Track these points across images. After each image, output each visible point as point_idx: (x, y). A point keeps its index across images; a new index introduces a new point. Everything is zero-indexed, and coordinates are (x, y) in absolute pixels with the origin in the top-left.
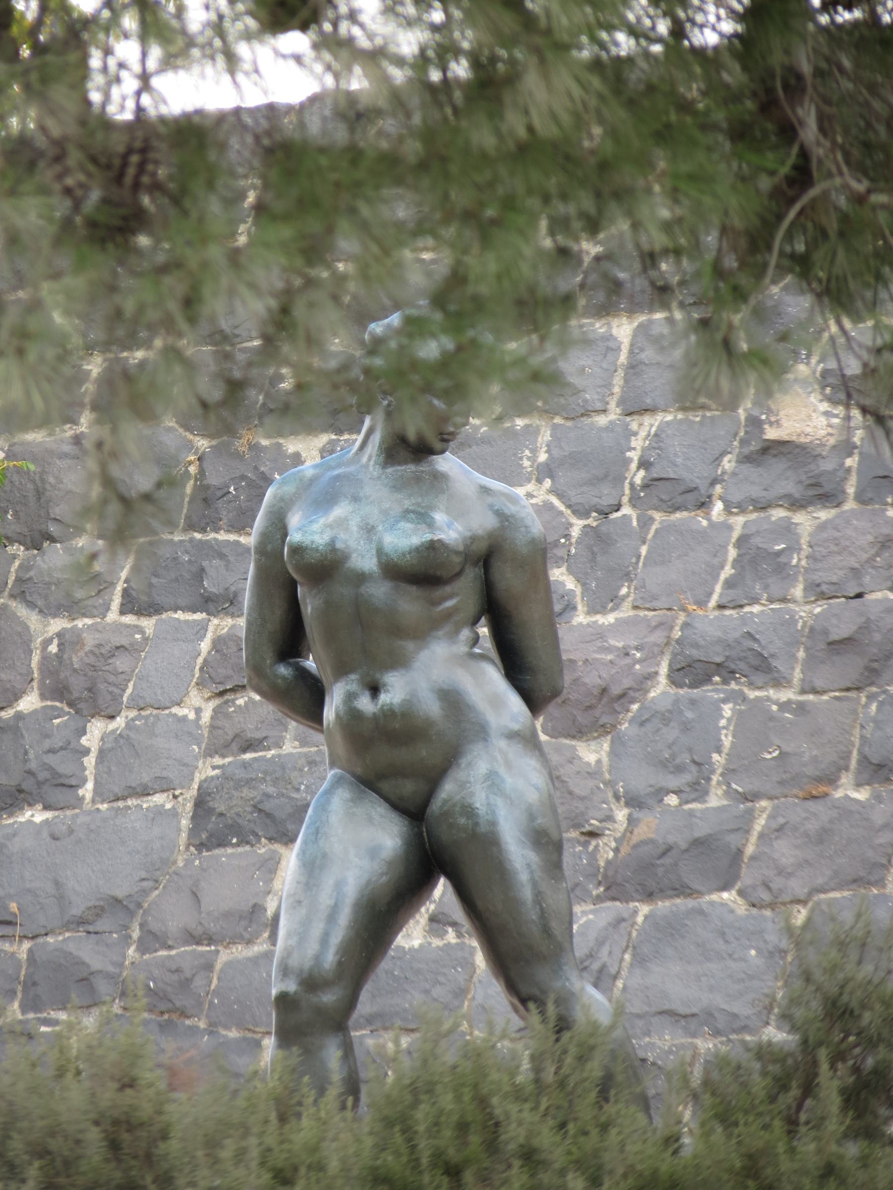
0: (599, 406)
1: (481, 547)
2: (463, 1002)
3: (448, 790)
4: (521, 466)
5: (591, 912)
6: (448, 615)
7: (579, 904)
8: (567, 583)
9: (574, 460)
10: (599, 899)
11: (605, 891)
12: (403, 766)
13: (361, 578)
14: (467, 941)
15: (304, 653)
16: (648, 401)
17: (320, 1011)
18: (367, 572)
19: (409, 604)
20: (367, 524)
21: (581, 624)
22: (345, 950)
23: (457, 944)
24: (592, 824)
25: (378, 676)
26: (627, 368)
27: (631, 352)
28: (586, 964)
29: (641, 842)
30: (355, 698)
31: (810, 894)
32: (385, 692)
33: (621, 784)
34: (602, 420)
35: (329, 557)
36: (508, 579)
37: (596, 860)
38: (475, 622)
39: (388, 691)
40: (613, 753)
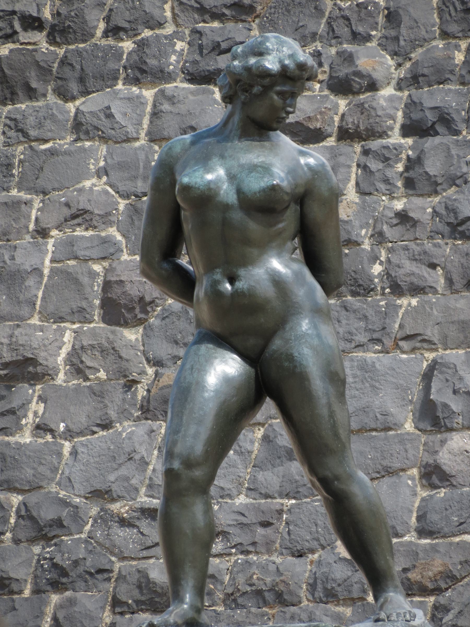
0: (135, 135)
1: (301, 190)
2: (56, 475)
3: (277, 344)
4: (89, 168)
5: (134, 425)
6: (280, 233)
7: (126, 420)
8: (117, 237)
9: (122, 166)
10: (138, 419)
11: (141, 414)
12: (248, 328)
13: (227, 207)
14: (58, 440)
15: (178, 256)
16: (166, 133)
17: (193, 481)
18: (230, 204)
19: (254, 227)
20: (230, 173)
21: (126, 260)
22: (209, 442)
23: (52, 442)
24: (133, 376)
25: (235, 270)
26: (152, 114)
27: (154, 106)
28: (131, 456)
29: (164, 386)
30: (219, 284)
31: (267, 419)
32: (239, 281)
33: (151, 353)
34: (137, 144)
35: (206, 193)
36: (316, 211)
37: (136, 396)
38: (293, 239)
39: (241, 280)
40: (146, 335)
